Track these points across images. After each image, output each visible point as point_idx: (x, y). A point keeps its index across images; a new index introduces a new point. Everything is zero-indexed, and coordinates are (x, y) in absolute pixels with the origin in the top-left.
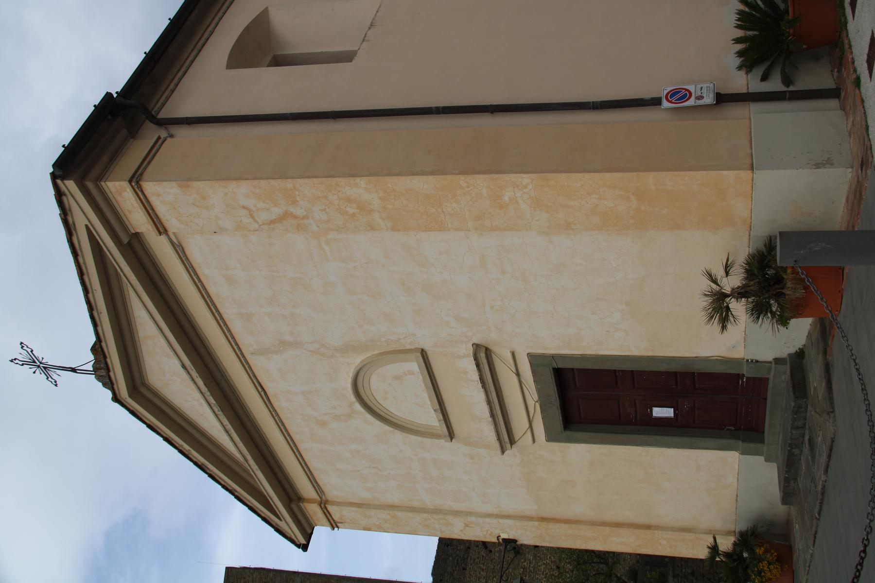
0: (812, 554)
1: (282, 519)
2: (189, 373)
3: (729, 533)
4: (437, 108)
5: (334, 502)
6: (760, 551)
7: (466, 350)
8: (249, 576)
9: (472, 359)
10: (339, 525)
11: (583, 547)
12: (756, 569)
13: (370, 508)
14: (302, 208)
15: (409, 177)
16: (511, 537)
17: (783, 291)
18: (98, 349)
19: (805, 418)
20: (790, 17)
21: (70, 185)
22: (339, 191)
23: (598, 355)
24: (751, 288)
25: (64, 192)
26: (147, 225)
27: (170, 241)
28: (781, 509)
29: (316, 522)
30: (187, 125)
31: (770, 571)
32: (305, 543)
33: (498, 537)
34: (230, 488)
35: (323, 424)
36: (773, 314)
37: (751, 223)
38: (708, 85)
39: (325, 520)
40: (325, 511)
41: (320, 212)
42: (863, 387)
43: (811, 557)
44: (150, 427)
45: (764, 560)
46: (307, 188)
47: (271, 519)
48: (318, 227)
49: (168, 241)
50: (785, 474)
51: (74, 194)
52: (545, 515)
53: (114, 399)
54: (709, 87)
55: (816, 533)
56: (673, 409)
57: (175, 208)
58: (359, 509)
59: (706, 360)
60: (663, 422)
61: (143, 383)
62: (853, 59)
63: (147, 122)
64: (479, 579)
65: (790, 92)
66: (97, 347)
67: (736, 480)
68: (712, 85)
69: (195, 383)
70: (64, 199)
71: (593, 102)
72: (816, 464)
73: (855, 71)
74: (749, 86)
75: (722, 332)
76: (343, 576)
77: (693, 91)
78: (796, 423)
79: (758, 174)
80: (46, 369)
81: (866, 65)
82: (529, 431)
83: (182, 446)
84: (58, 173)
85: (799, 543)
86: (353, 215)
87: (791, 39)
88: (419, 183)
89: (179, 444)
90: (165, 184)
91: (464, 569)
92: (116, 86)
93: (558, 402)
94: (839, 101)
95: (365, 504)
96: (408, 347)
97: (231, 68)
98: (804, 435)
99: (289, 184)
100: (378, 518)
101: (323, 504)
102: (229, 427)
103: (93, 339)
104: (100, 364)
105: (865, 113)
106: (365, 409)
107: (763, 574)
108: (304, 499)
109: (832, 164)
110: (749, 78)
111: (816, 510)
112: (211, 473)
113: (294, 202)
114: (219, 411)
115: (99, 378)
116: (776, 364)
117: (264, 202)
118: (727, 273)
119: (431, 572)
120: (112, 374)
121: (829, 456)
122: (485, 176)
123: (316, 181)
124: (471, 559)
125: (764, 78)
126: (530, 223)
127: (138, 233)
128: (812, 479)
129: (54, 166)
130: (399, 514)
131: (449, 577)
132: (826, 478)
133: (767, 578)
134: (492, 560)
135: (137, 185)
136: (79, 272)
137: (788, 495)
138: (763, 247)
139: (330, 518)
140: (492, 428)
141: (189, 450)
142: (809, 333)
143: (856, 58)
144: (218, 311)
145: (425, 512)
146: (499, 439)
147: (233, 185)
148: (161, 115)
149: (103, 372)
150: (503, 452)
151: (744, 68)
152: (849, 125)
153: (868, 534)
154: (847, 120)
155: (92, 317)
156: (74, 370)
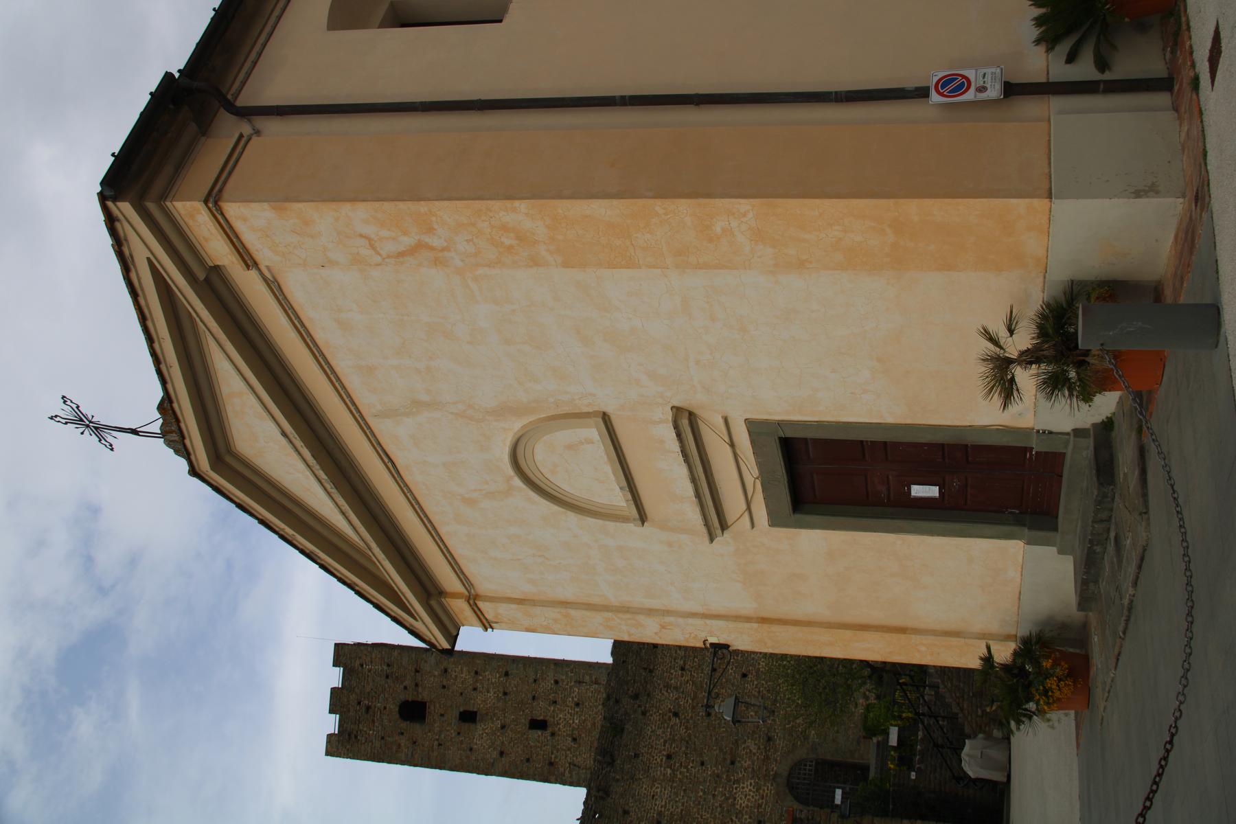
0: (1113, 678)
1: (418, 618)
2: (291, 442)
3: (1008, 638)
4: (623, 97)
6: (1047, 664)
7: (663, 414)
8: (366, 655)
9: (671, 425)
10: (493, 625)
11: (817, 654)
12: (1041, 688)
13: (535, 605)
14: (440, 238)
15: (586, 201)
16: (722, 641)
17: (1088, 359)
18: (167, 406)
19: (1111, 510)
21: (125, 208)
22: (491, 217)
23: (839, 422)
24: (1045, 353)
25: (117, 217)
26: (229, 256)
27: (262, 277)
29: (464, 622)
30: (279, 117)
31: (1060, 690)
32: (449, 647)
33: (705, 641)
34: (349, 582)
35: (469, 502)
37: (1047, 263)
39: (474, 619)
40: (476, 609)
41: (465, 242)
42: (1181, 523)
43: (1112, 681)
45: (1052, 676)
46: (447, 213)
47: (403, 619)
48: (462, 261)
49: (260, 277)
50: (1084, 575)
51: (130, 220)
53: (191, 472)
54: (995, 74)
56: (938, 487)
57: (267, 236)
58: (520, 606)
59: (984, 429)
60: (925, 446)
61: (229, 451)
62: (1191, 47)
63: (222, 110)
64: (675, 660)
66: (165, 405)
67: (1019, 574)
68: (998, 71)
69: (300, 454)
70: (118, 225)
71: (836, 93)
73: (1193, 65)
75: (1004, 409)
76: (492, 654)
77: (972, 80)
78: (1099, 515)
79: (1060, 206)
80: (98, 430)
81: (1208, 75)
82: (746, 514)
83: (283, 530)
84: (107, 193)
86: (510, 247)
87: (1108, 9)
88: (600, 209)
90: (253, 205)
93: (785, 477)
94: (1172, 95)
95: (528, 600)
96: (585, 410)
98: (1108, 530)
99: (423, 207)
100: (546, 618)
101: (473, 599)
102: (346, 507)
103: (159, 394)
104: (171, 427)
105: (1203, 131)
106: (526, 485)
107: (1050, 694)
108: (446, 593)
109: (1157, 192)
111: (1121, 628)
112: (322, 562)
113: (431, 230)
114: (332, 488)
115: (169, 443)
117: (389, 230)
118: (1011, 332)
120: (187, 442)
121: (1140, 567)
122: (689, 201)
125: (1071, 58)
126: (750, 260)
127: (218, 266)
128: (1117, 588)
129: (102, 183)
130: (573, 612)
131: (635, 657)
132: (1134, 592)
133: (1055, 699)
135: (215, 206)
136: (140, 316)
137: (1086, 598)
139: (482, 617)
140: (697, 510)
141: (293, 535)
143: (1195, 47)
145: (608, 611)
146: (707, 524)
147: (346, 208)
148: (241, 102)
149: (174, 437)
150: (712, 540)
152: (1183, 135)
153: (1177, 719)
154: (1181, 125)
156: (134, 432)
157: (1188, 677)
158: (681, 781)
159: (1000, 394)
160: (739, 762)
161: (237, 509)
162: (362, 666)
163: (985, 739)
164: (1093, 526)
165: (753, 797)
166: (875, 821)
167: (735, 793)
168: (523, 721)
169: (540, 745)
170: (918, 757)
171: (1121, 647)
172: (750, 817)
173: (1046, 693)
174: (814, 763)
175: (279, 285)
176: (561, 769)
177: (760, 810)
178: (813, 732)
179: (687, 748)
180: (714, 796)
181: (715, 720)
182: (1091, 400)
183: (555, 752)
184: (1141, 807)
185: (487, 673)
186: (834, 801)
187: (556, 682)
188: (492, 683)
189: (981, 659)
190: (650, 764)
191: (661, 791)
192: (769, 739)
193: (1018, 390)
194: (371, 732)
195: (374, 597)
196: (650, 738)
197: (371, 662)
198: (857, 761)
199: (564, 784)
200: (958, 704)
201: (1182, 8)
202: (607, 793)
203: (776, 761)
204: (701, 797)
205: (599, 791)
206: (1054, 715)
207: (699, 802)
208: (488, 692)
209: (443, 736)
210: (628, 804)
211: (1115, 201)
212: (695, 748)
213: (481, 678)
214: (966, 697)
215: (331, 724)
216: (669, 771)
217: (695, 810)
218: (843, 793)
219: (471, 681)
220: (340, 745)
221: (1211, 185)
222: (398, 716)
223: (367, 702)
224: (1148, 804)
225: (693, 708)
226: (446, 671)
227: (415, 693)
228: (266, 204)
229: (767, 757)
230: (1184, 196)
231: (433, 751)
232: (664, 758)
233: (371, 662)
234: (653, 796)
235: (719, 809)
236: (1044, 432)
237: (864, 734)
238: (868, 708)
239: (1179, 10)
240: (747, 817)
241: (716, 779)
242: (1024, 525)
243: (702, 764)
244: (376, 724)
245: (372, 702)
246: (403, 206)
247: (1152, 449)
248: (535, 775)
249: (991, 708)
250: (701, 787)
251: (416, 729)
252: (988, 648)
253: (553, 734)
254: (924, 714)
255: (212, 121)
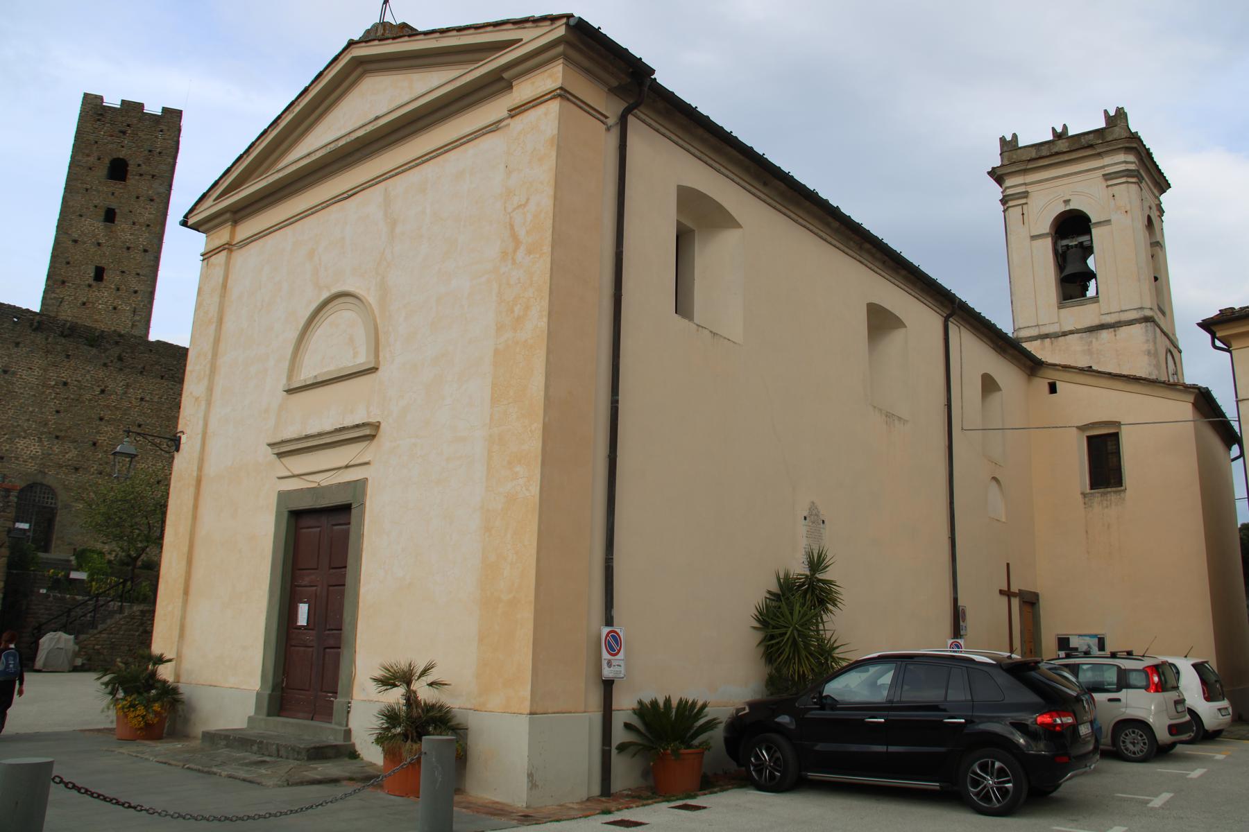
4: (617, 401)
5: (230, 258)
8: (170, 135)
9: (365, 421)
10: (206, 261)
12: (137, 703)
13: (221, 296)
18: (405, 31)
19: (287, 758)
20: (683, 751)
21: (560, 31)
26: (519, 98)
28: (199, 729)
29: (211, 237)
31: (135, 717)
32: (189, 224)
33: (182, 432)
34: (251, 150)
36: (387, 729)
38: (623, 672)
39: (212, 247)
40: (221, 249)
44: (320, 75)
45: (147, 711)
46: (541, 266)
48: (504, 273)
51: (552, 32)
52: (204, 484)
55: (170, 764)
59: (353, 662)
60: (291, 614)
62: (632, 807)
63: (626, 105)
65: (610, 751)
68: (622, 676)
70: (549, 23)
71: (613, 559)
72: (238, 767)
73: (619, 810)
74: (621, 712)
77: (617, 657)
79: (525, 719)
81: (612, 820)
82: (290, 474)
83: (298, 105)
85: (161, 747)
86: (513, 311)
89: (301, 102)
91: (162, 377)
92: (661, 78)
94: (599, 796)
96: (381, 354)
97: (678, 190)
98: (269, 756)
99: (547, 249)
101: (228, 247)
102: (313, 157)
105: (574, 819)
107: (132, 709)
109: (531, 789)
110: (628, 711)
111: (192, 766)
112: (269, 132)
113: (529, 252)
114: (330, 148)
115: (375, 27)
116: (345, 731)
118: (431, 685)
119: (161, 340)
120: (376, 42)
121: (244, 780)
123: (548, 276)
124: (173, 385)
125: (628, 726)
128: (225, 763)
130: (213, 328)
134: (170, 408)
137: (212, 738)
138: (456, 723)
142: (375, 764)
143: (631, 810)
144: (431, 159)
146: (283, 442)
147: (550, 191)
148: (631, 119)
150: (269, 445)
151: (639, 707)
152: (571, 805)
155: (433, 32)
157: (167, 817)
158: (44, 392)
159: (384, 676)
160: (58, 443)
161: (319, 72)
162: (161, 131)
163: (74, 651)
164: (274, 744)
165: (25, 453)
166: (4, 558)
167: (30, 439)
168: (103, 262)
169: (81, 274)
170: (59, 595)
171: (176, 766)
172: (7, 450)
173: (133, 706)
174: (53, 506)
175: (494, 131)
176: (58, 291)
177: (13, 459)
178: (81, 506)
179: (73, 399)
180: (28, 420)
181: (96, 424)
182: (378, 744)
183: (74, 286)
184: (80, 786)
185: (147, 234)
186: (18, 522)
187: (136, 292)
188: (138, 238)
189: (162, 655)
190: (61, 367)
191: (34, 375)
192: (77, 469)
193: (387, 689)
194: (102, 133)
195: (235, 170)
196: (83, 369)
197: (164, 139)
198: (54, 543)
199: (46, 292)
200: (105, 630)
201: (657, 800)
202: (36, 330)
203: (57, 474)
204: (28, 409)
205: (38, 322)
206: (112, 714)
207: (23, 408)
208: (131, 234)
209: (94, 193)
210: (25, 347)
211: (526, 759)
212: (72, 406)
213: (144, 229)
214: (111, 636)
215: (112, 100)
216: (53, 383)
217: (16, 404)
218: (25, 530)
219: (141, 220)
220: (93, 108)
221: (537, 826)
222: (115, 157)
223: (129, 132)
224: (83, 791)
225: (108, 407)
226: (152, 200)
227: (134, 173)
228: (557, 132)
229: (60, 466)
230: (527, 807)
231: (81, 183)
232: (64, 380)
233: (164, 139)
234: (31, 369)
235: (15, 424)
236: (349, 707)
237: (78, 550)
238: (101, 553)
239: (656, 798)
240: (7, 448)
241: (44, 423)
242: (273, 691)
243: (58, 412)
244: (109, 138)
245: (128, 136)
246: (549, 234)
247: (339, 790)
248: (55, 268)
249: (120, 662)
250: (37, 410)
251: (102, 171)
252: (170, 660)
253: (90, 286)
254: (97, 601)
255: (618, 96)
